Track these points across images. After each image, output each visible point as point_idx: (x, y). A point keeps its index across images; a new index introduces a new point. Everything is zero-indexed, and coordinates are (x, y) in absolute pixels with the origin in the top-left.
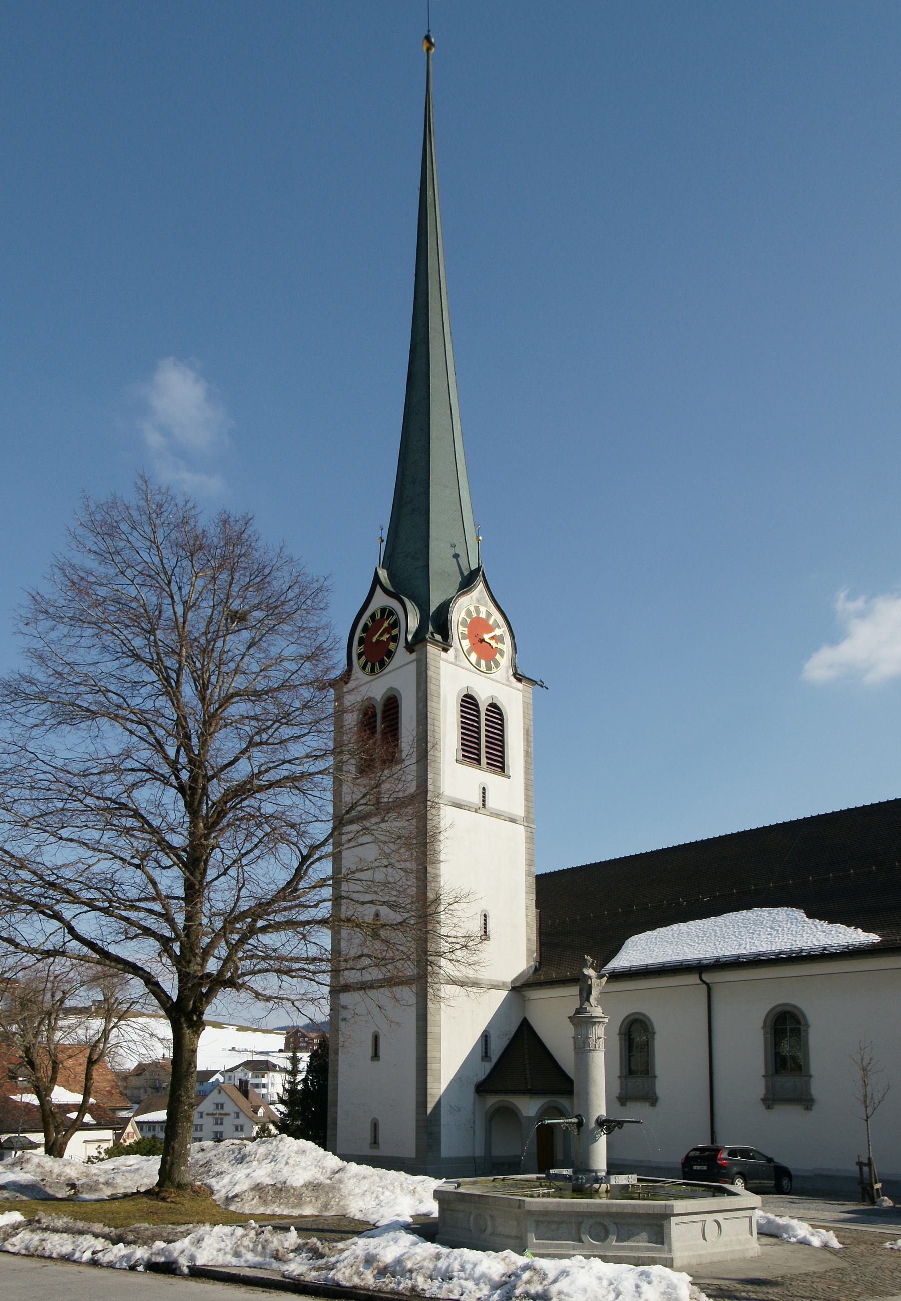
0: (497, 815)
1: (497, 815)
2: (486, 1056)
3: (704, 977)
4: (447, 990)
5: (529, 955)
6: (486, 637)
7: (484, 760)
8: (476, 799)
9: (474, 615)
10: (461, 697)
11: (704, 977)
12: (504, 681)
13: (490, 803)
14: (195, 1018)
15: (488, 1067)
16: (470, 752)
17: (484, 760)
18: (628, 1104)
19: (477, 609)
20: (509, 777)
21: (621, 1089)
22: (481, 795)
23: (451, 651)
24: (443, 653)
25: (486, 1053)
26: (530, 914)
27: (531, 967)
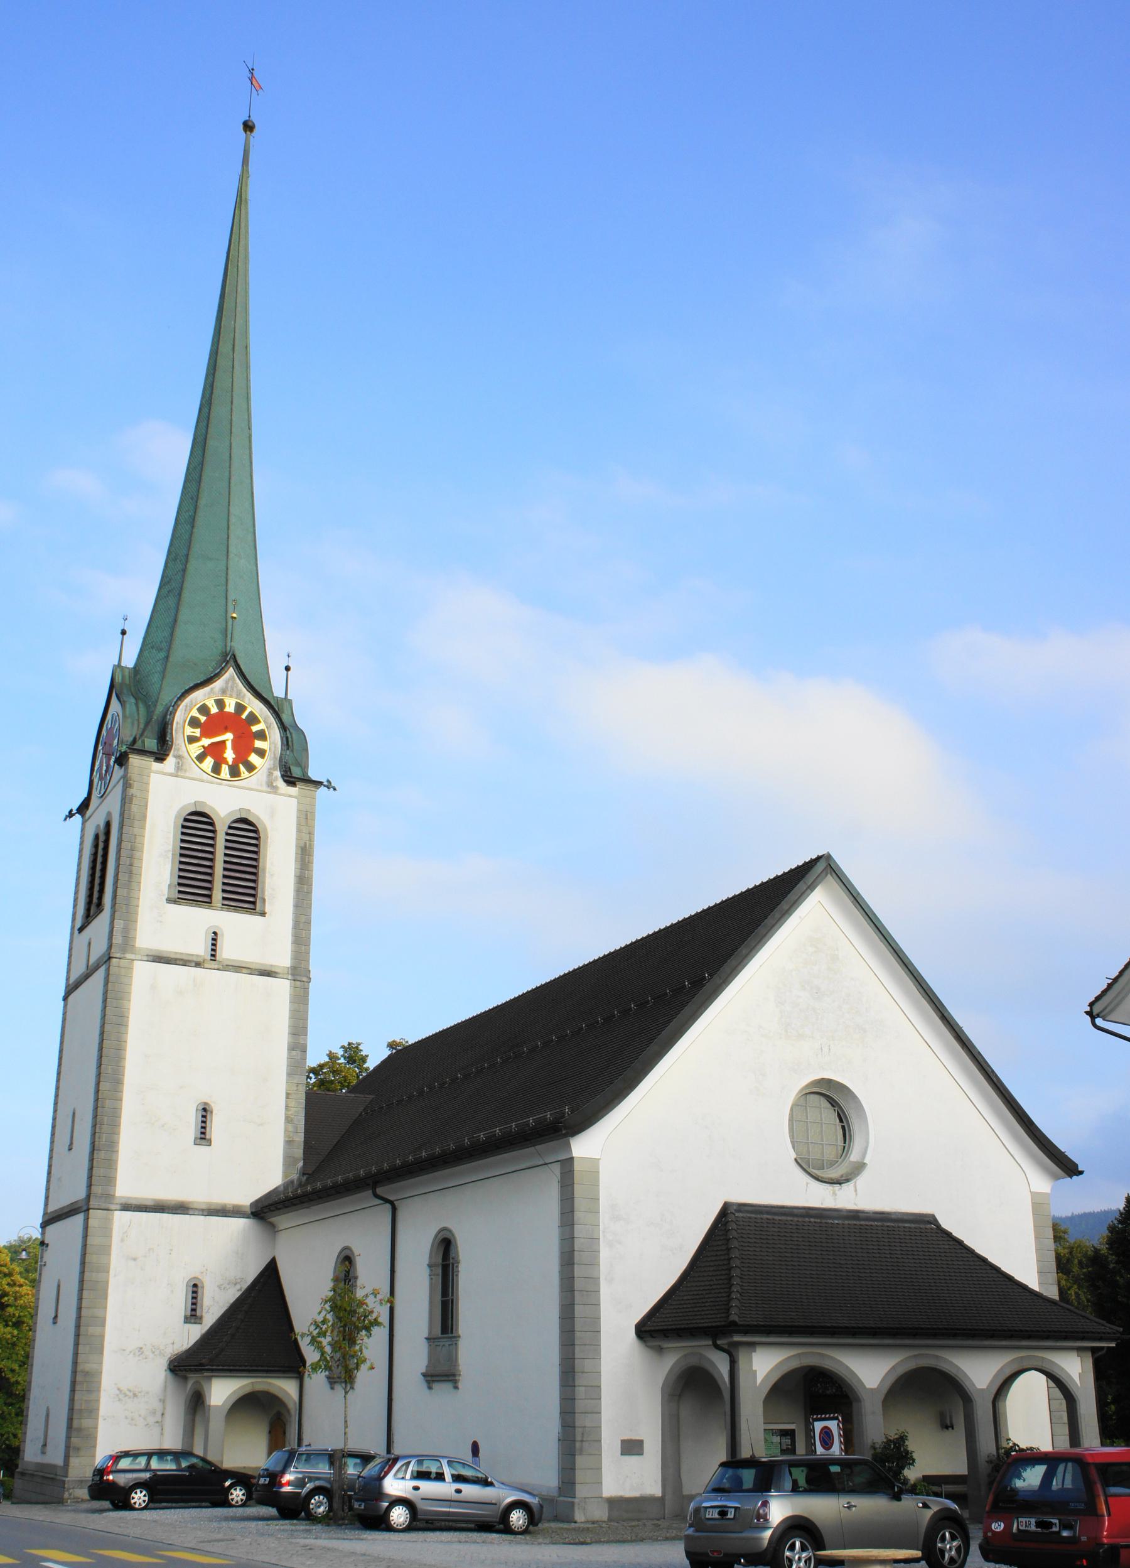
0: (238, 968)
1: (238, 968)
2: (193, 1316)
3: (379, 1191)
4: (121, 1219)
5: (288, 1160)
6: (228, 737)
7: (218, 895)
8: (201, 949)
9: (203, 719)
10: (181, 821)
11: (379, 1191)
12: (265, 788)
13: (226, 952)
14: (227, 1484)
15: (195, 1332)
16: (192, 886)
17: (218, 895)
18: (436, 1386)
19: (220, 703)
20: (263, 914)
21: (430, 1360)
22: (210, 942)
23: (171, 761)
24: (156, 766)
25: (193, 1310)
26: (292, 1104)
27: (292, 1182)
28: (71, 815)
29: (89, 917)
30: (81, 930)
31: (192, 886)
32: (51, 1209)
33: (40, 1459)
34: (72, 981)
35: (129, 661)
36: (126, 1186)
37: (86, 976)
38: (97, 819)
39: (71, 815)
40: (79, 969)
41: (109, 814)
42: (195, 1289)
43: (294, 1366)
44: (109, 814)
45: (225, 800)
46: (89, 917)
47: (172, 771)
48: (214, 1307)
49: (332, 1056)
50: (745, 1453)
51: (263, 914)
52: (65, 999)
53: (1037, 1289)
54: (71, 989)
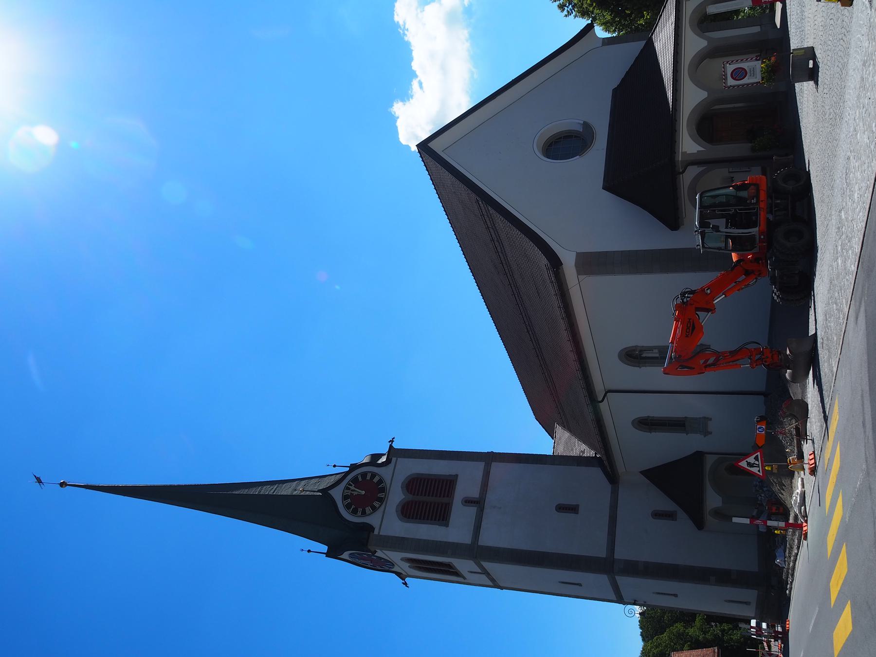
2: (669, 516)
8: (473, 510)
13: (475, 493)
15: (681, 514)
16: (440, 514)
24: (376, 532)
28: (405, 584)
29: (457, 574)
30: (465, 578)
31: (440, 514)
32: (614, 598)
33: (754, 605)
34: (491, 584)
35: (324, 548)
36: (602, 553)
37: (488, 574)
38: (405, 567)
39: (405, 584)
40: (484, 579)
41: (402, 559)
42: (657, 515)
43: (699, 456)
44: (402, 559)
45: (396, 496)
46: (457, 574)
47: (331, 492)
48: (666, 504)
49: (576, 16)
50: (666, 333)
51: (457, 476)
52: (502, 588)
53: (549, 452)
54: (496, 585)
